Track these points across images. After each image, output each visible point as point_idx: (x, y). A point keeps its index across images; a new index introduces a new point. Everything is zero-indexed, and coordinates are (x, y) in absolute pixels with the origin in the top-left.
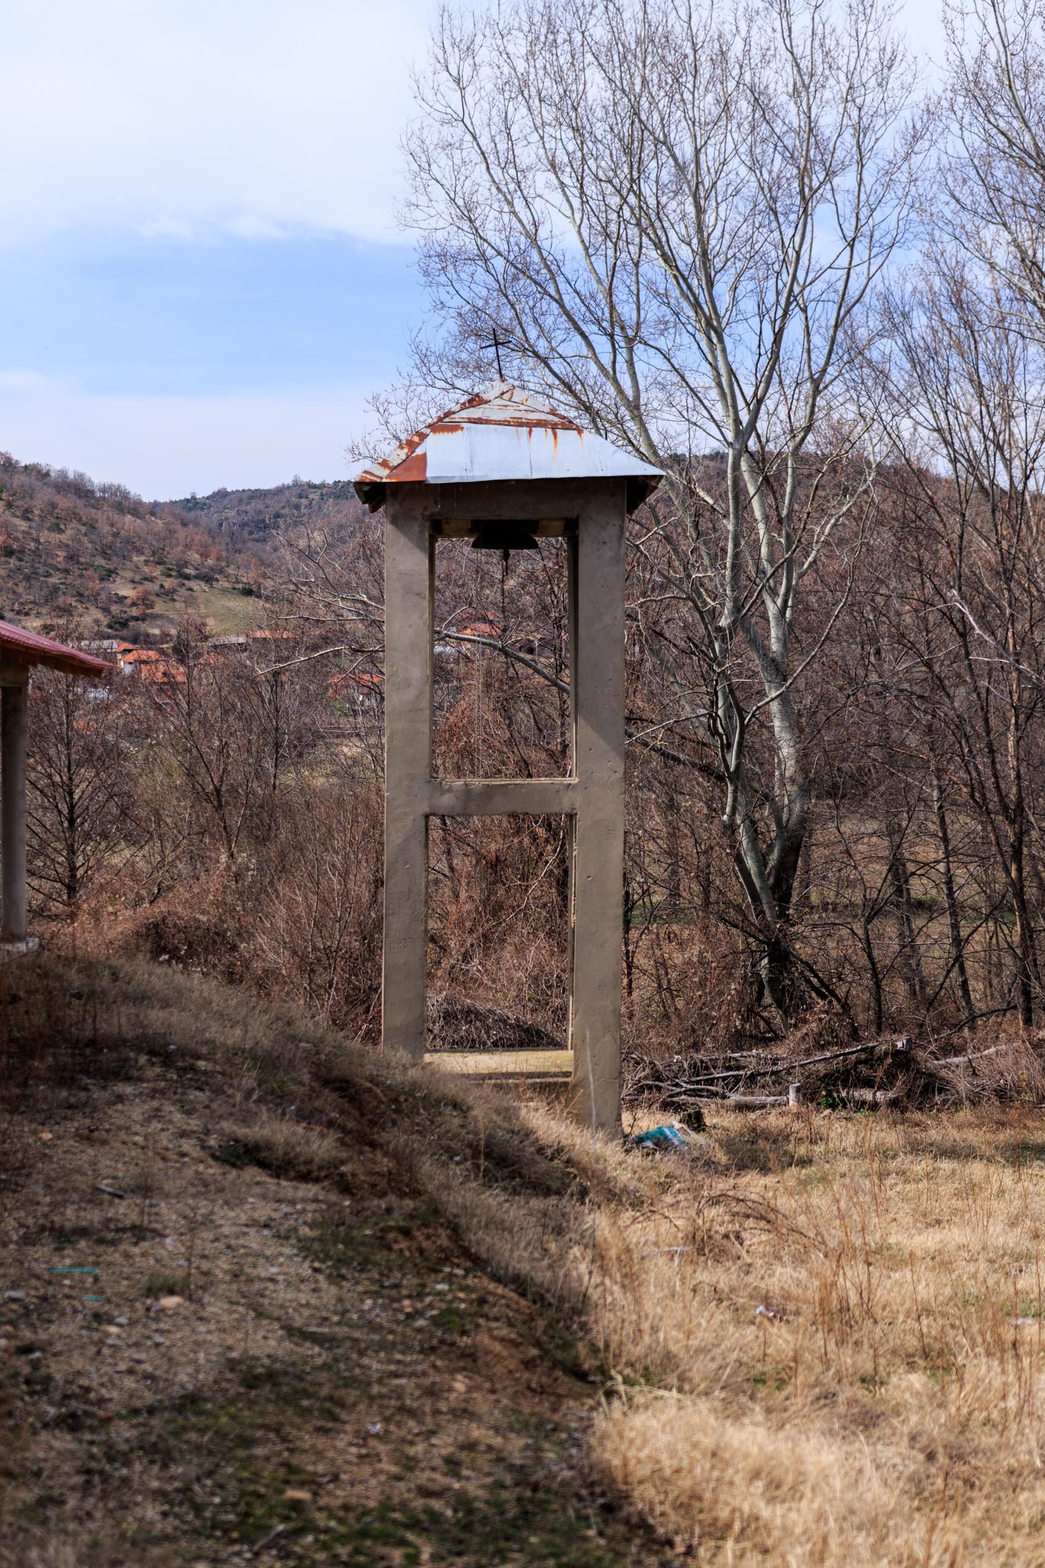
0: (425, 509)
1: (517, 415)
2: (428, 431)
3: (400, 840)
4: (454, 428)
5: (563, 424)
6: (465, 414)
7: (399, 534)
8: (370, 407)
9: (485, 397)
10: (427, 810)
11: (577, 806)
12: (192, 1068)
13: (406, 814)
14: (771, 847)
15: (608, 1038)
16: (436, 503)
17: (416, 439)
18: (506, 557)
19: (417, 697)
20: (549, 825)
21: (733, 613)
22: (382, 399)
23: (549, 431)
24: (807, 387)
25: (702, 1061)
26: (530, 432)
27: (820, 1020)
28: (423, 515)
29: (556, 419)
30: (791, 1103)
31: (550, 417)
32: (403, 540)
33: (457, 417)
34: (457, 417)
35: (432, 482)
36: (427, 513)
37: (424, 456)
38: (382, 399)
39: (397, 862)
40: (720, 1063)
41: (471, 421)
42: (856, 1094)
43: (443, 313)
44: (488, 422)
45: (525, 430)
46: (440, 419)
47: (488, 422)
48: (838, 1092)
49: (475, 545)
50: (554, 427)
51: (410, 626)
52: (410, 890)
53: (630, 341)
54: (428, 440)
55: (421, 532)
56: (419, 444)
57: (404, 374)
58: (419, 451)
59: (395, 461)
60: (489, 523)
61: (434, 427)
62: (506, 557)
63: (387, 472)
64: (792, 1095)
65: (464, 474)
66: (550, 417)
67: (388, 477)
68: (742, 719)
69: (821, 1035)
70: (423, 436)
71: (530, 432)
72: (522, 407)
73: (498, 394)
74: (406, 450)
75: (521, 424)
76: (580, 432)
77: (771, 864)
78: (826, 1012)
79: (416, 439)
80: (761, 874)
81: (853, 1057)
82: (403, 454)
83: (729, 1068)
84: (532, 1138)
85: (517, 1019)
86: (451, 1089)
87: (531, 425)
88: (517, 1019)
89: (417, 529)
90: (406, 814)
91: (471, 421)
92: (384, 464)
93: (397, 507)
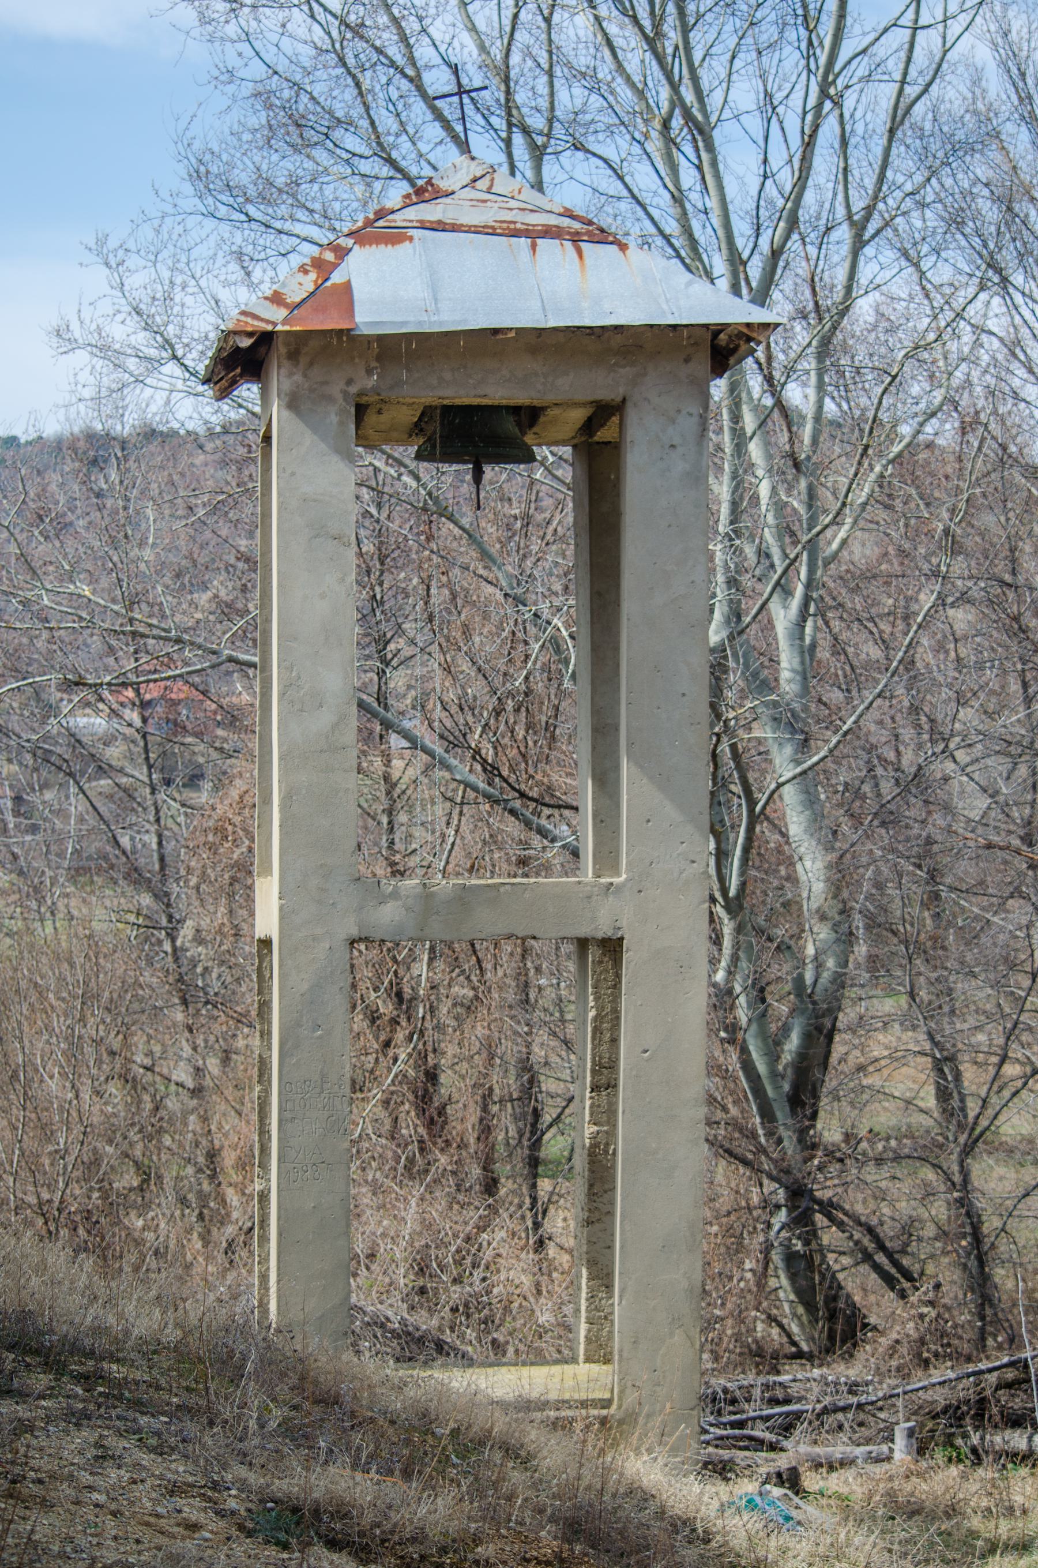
0: (350, 382)
1: (508, 216)
2: (350, 242)
3: (305, 986)
4: (396, 237)
5: (589, 233)
6: (413, 214)
7: (301, 426)
8: (92, 258)
9: (444, 185)
10: (355, 932)
11: (624, 923)
12: (100, 1376)
13: (315, 939)
14: (786, 1030)
15: (678, 1337)
16: (369, 372)
17: (329, 256)
18: (478, 476)
19: (335, 726)
20: (399, 995)
21: (728, 621)
22: (112, 243)
23: (568, 245)
24: (843, 233)
25: (725, 1391)
26: (534, 247)
27: (922, 1316)
28: (345, 393)
29: (577, 225)
30: (898, 1455)
31: (566, 222)
32: (309, 438)
33: (398, 219)
34: (398, 219)
35: (366, 331)
36: (353, 389)
37: (347, 287)
38: (112, 243)
39: (299, 1025)
40: (757, 1393)
41: (424, 226)
42: (998, 1439)
43: (231, 89)
44: (455, 228)
45: (524, 242)
46: (369, 223)
47: (455, 228)
48: (965, 1436)
49: (419, 457)
50: (576, 239)
51: (323, 596)
52: (324, 1077)
53: (538, 154)
54: (350, 258)
55: (341, 423)
56: (335, 266)
57: (164, 194)
58: (337, 278)
59: (295, 295)
60: (448, 411)
61: (361, 236)
62: (478, 476)
63: (282, 313)
64: (900, 1442)
65: (425, 318)
66: (566, 222)
67: (285, 322)
68: (752, 803)
69: (922, 1341)
70: (342, 253)
71: (534, 247)
72: (513, 204)
73: (466, 180)
74: (313, 276)
75: (516, 234)
76: (623, 247)
77: (787, 1057)
78: (931, 1303)
79: (329, 256)
80: (774, 1074)
81: (992, 1378)
82: (309, 281)
83: (774, 1402)
84: (652, 1507)
85: (403, 1322)
86: (500, 1424)
87: (534, 235)
88: (403, 1322)
89: (334, 419)
90: (315, 939)
91: (424, 226)
92: (277, 299)
93: (298, 378)
